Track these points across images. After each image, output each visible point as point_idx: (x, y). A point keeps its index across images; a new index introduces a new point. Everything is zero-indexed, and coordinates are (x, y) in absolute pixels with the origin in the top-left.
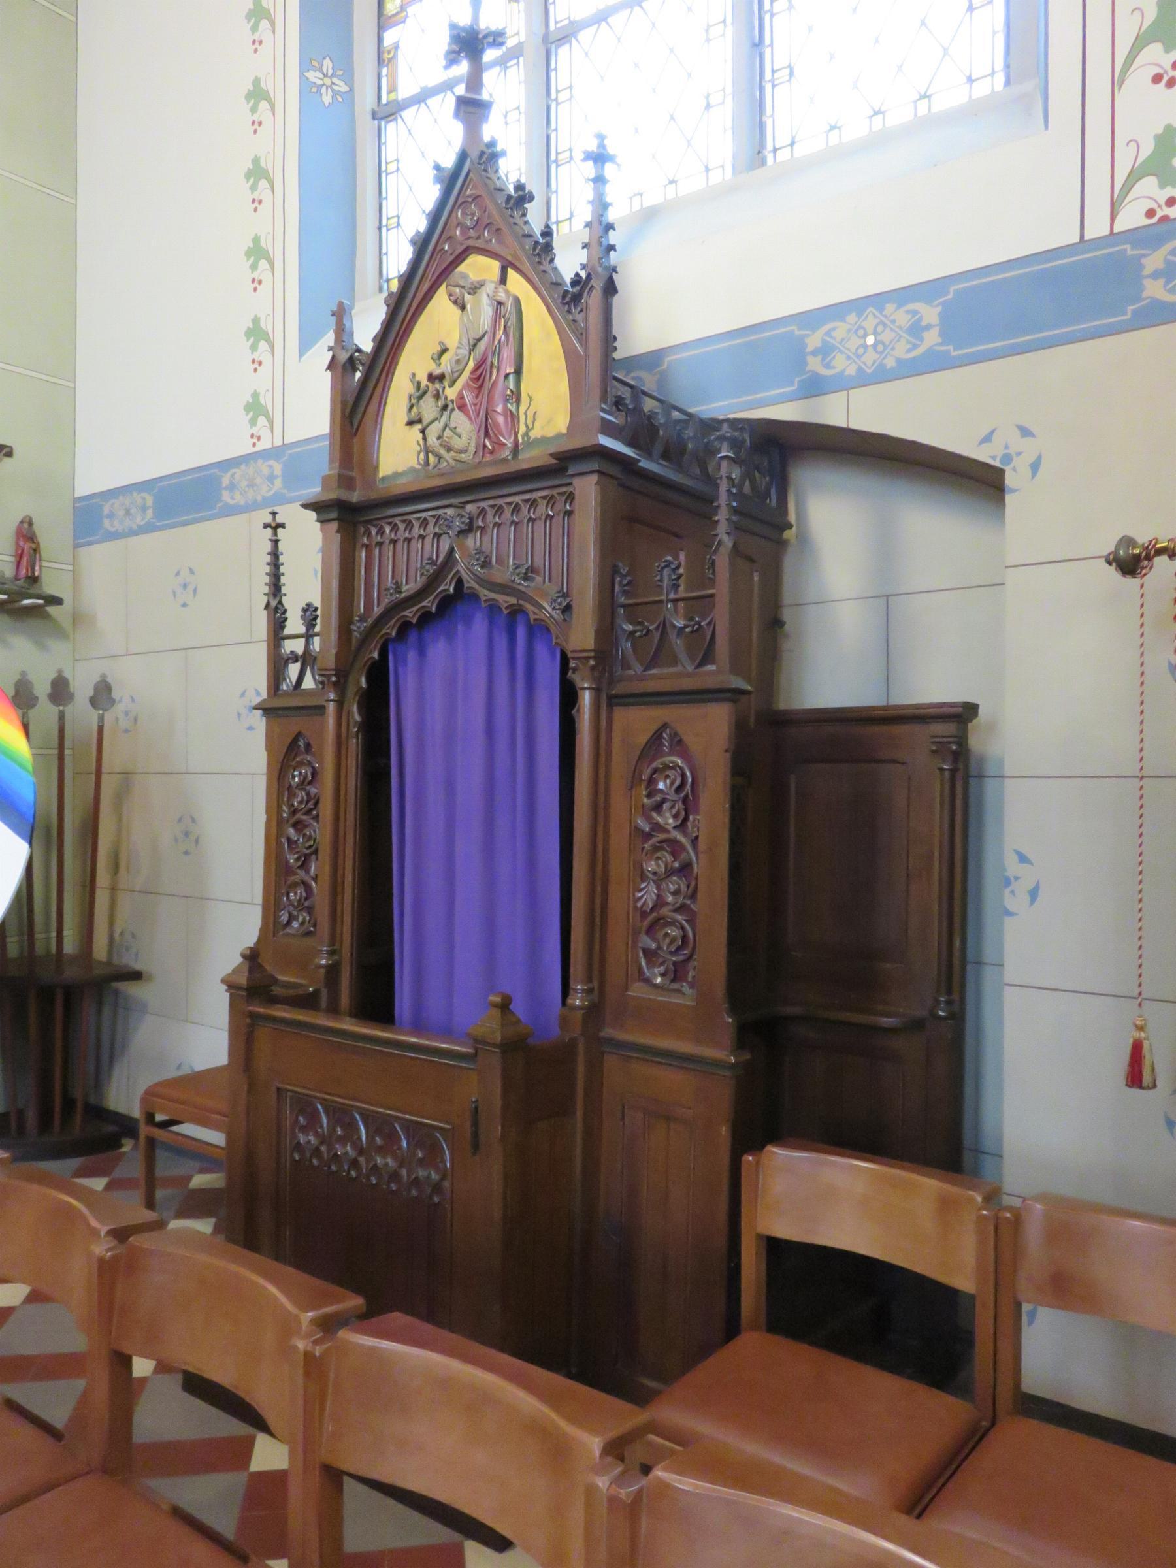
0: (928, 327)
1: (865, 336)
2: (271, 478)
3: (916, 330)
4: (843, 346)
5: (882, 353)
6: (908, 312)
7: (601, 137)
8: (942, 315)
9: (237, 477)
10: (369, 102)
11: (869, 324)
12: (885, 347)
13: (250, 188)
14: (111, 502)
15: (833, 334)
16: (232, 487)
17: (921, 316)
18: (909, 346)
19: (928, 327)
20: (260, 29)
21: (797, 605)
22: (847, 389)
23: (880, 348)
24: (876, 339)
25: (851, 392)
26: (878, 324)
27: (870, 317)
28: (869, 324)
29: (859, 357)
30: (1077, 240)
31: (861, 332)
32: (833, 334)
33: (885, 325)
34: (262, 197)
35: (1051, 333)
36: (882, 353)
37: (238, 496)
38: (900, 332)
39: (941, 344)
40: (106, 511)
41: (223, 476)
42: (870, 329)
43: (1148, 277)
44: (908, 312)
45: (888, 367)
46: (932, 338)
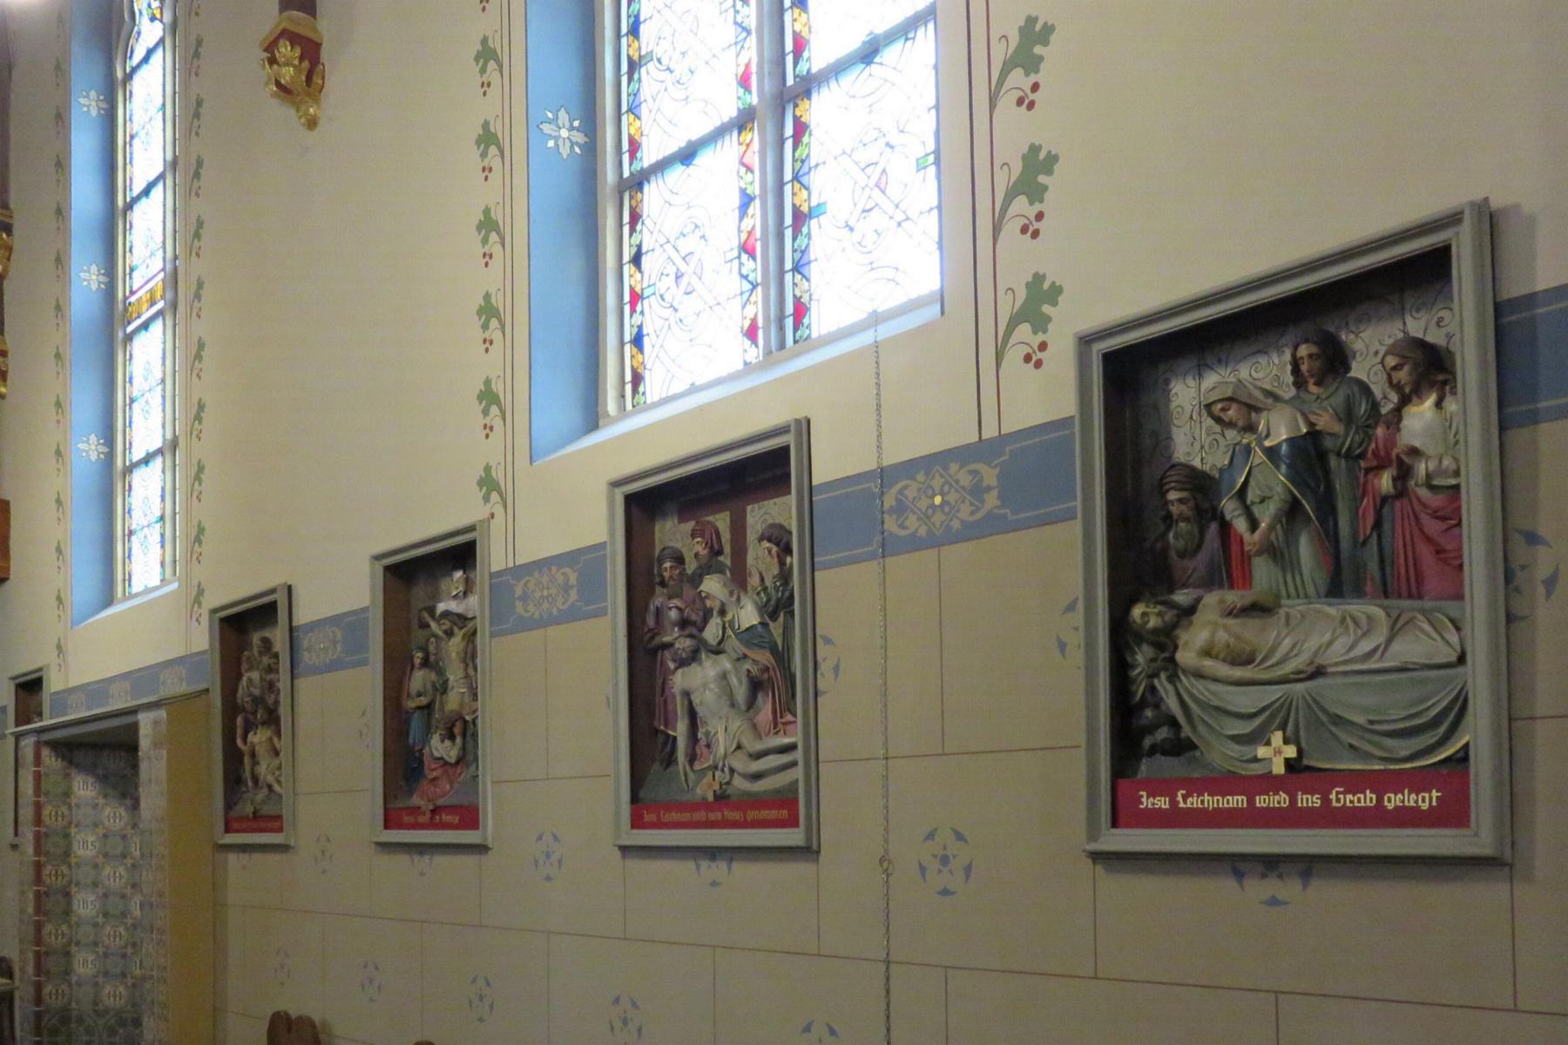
0: (989, 489)
1: (933, 497)
2: (566, 588)
3: (978, 491)
4: (915, 506)
5: (949, 514)
6: (970, 472)
7: (929, 109)
8: (999, 477)
9: (531, 585)
10: (610, 177)
11: (937, 483)
12: (952, 508)
13: (482, 327)
14: (523, 581)
15: (906, 492)
16: (900, 509)
17: (982, 477)
18: (971, 508)
19: (989, 489)
20: (490, 156)
21: (1511, 877)
22: (938, 546)
23: (947, 509)
24: (943, 499)
25: (941, 548)
26: (944, 484)
27: (937, 475)
28: (937, 483)
29: (928, 518)
30: (977, 439)
31: (930, 492)
32: (906, 492)
33: (951, 485)
34: (493, 337)
35: (1047, 510)
36: (949, 514)
37: (531, 608)
38: (913, 507)
39: (999, 508)
40: (518, 591)
41: (515, 585)
42: (937, 489)
43: (994, 488)
44: (970, 472)
45: (960, 527)
46: (992, 500)
